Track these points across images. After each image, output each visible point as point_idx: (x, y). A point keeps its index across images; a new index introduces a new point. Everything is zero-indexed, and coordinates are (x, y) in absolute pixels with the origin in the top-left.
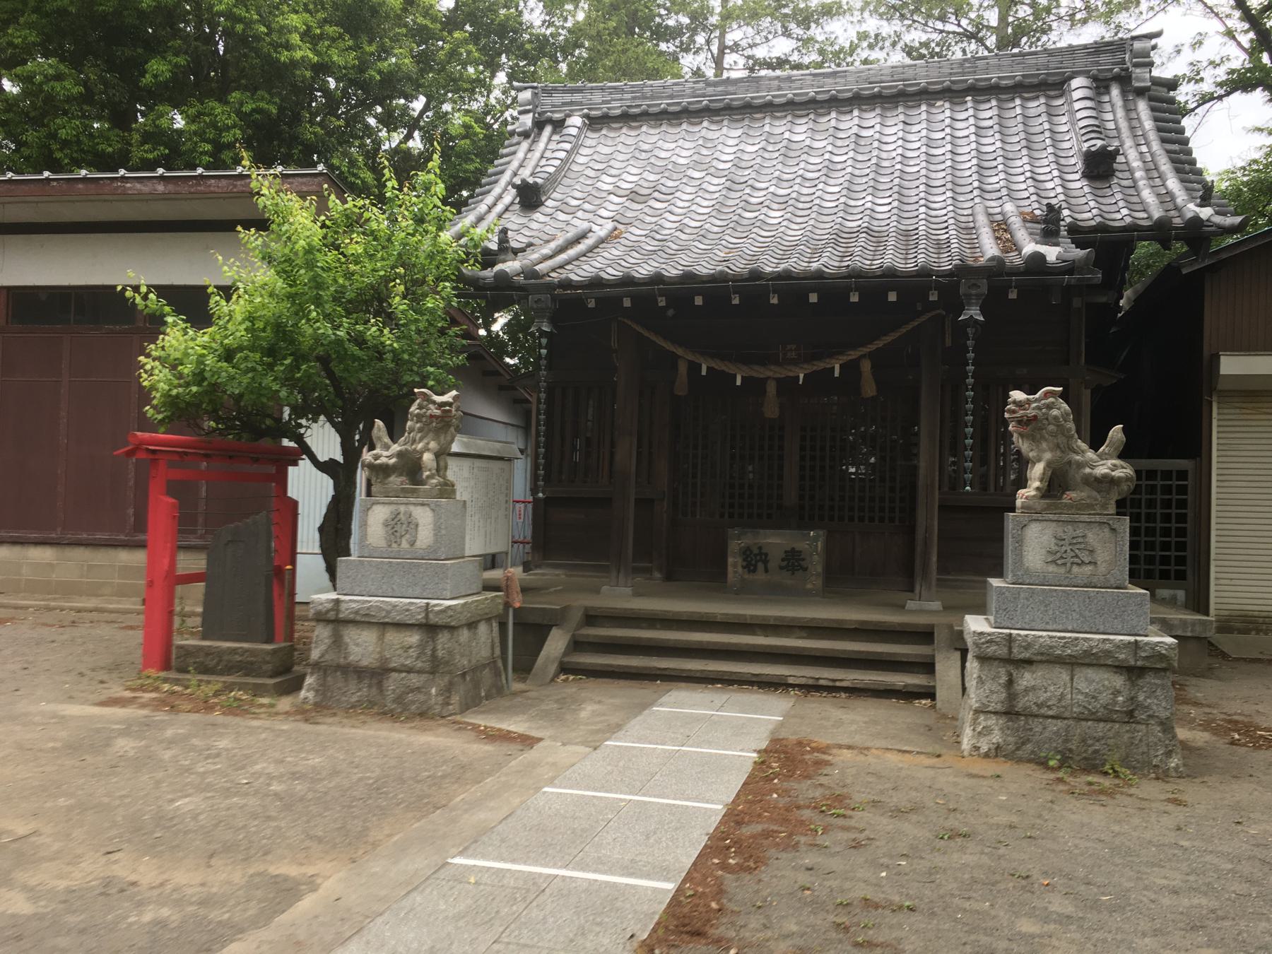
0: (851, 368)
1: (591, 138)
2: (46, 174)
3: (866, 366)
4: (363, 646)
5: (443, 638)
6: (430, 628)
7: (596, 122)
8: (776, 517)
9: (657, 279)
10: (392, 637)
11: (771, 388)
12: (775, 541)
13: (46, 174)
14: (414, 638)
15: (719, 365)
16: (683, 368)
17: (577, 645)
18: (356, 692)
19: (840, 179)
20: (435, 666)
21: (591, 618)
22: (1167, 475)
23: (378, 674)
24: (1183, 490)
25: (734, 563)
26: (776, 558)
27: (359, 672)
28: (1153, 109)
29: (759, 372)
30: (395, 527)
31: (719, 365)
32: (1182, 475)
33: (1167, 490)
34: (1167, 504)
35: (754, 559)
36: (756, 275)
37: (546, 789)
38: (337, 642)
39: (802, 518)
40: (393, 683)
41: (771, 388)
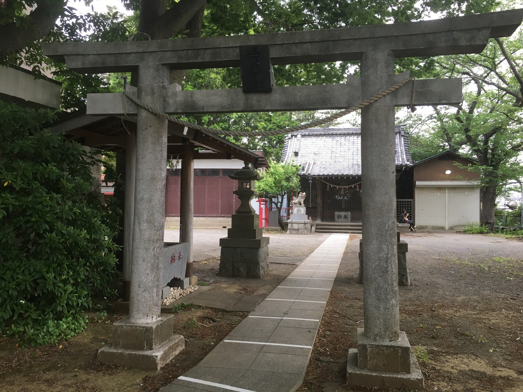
0: (355, 187)
1: (303, 139)
2: (69, 111)
3: (358, 186)
4: (295, 226)
5: (307, 225)
6: (305, 224)
7: (303, 136)
8: (342, 210)
9: (328, 175)
10: (299, 225)
11: (343, 189)
12: (343, 214)
13: (69, 111)
14: (303, 225)
15: (334, 186)
16: (328, 186)
17: (316, 229)
18: (295, 232)
19: (351, 151)
20: (306, 228)
21: (317, 225)
22: (408, 202)
23: (298, 230)
24: (411, 204)
25: (336, 217)
26: (343, 216)
27: (295, 230)
28: (404, 139)
29: (341, 187)
30: (298, 211)
31: (334, 186)
32: (411, 202)
33: (403, 204)
34: (408, 207)
35: (339, 217)
36: (343, 175)
37: (181, 378)
38: (292, 226)
39: (346, 210)
40: (300, 231)
41: (343, 189)
